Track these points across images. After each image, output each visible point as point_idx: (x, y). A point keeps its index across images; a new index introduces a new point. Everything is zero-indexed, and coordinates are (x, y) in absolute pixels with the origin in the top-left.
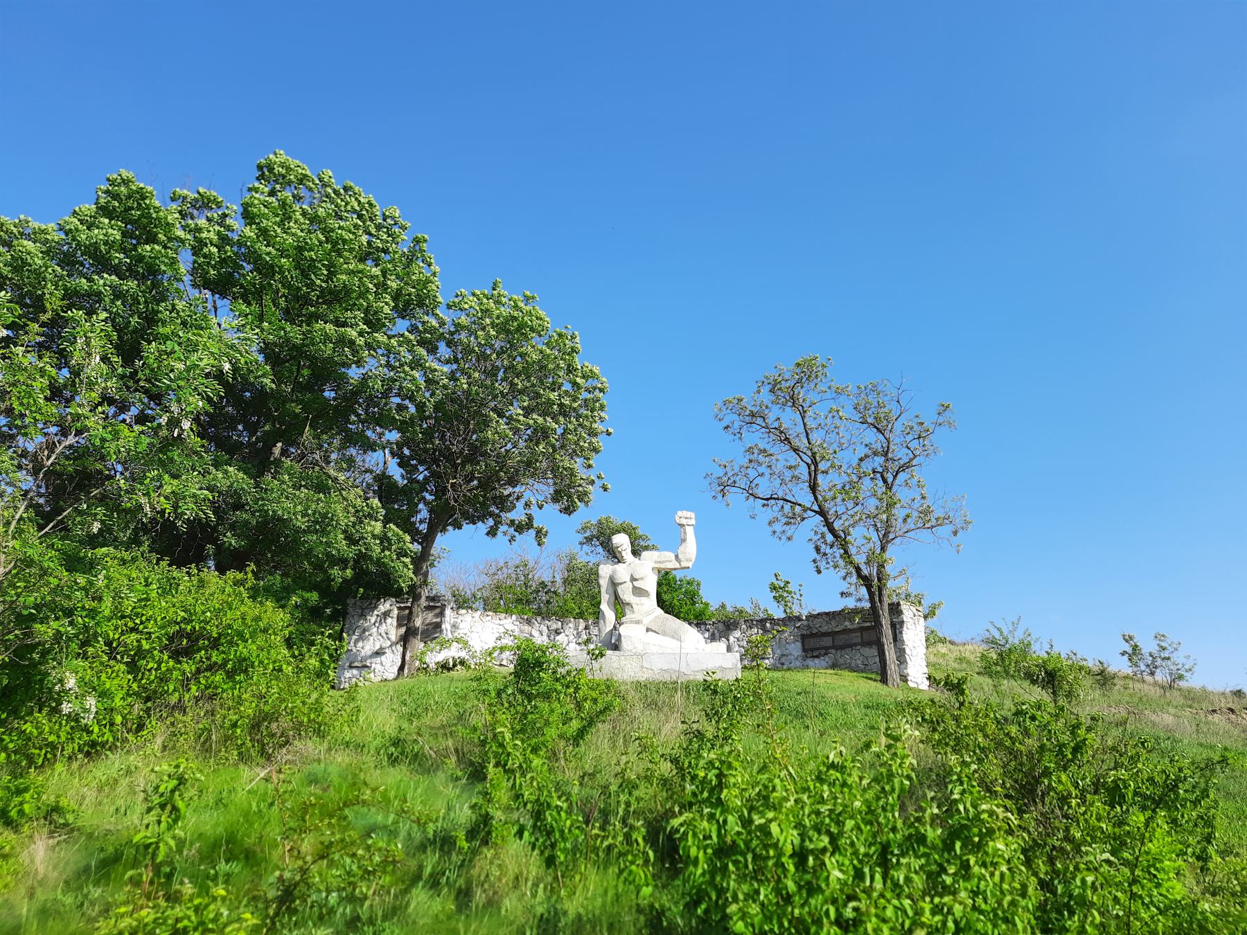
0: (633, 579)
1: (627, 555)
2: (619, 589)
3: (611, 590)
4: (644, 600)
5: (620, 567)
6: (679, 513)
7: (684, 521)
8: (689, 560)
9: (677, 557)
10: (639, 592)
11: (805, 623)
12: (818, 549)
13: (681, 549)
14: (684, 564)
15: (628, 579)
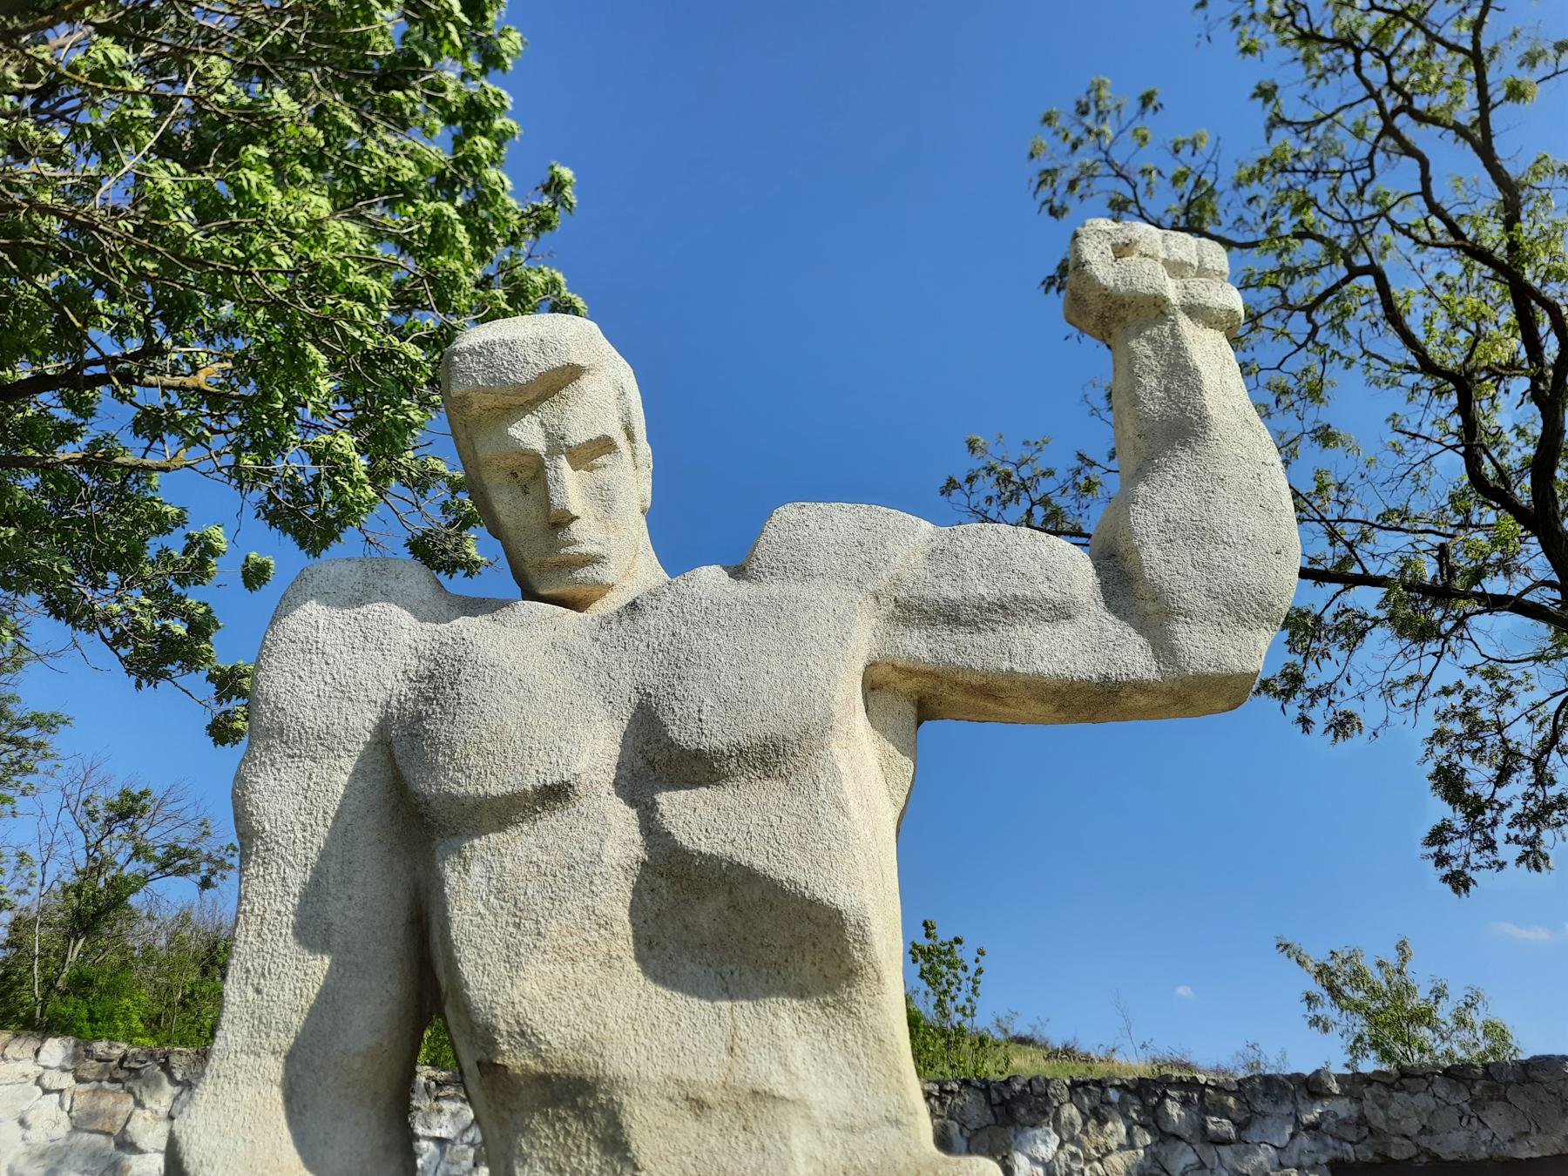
0: (658, 760)
1: (611, 515)
2: (471, 888)
3: (371, 897)
4: (782, 1041)
5: (517, 645)
8: (1239, 608)
9: (1121, 581)
10: (728, 930)
11: (1344, 1108)
12: (1449, 782)
14: (1208, 646)
15: (593, 751)
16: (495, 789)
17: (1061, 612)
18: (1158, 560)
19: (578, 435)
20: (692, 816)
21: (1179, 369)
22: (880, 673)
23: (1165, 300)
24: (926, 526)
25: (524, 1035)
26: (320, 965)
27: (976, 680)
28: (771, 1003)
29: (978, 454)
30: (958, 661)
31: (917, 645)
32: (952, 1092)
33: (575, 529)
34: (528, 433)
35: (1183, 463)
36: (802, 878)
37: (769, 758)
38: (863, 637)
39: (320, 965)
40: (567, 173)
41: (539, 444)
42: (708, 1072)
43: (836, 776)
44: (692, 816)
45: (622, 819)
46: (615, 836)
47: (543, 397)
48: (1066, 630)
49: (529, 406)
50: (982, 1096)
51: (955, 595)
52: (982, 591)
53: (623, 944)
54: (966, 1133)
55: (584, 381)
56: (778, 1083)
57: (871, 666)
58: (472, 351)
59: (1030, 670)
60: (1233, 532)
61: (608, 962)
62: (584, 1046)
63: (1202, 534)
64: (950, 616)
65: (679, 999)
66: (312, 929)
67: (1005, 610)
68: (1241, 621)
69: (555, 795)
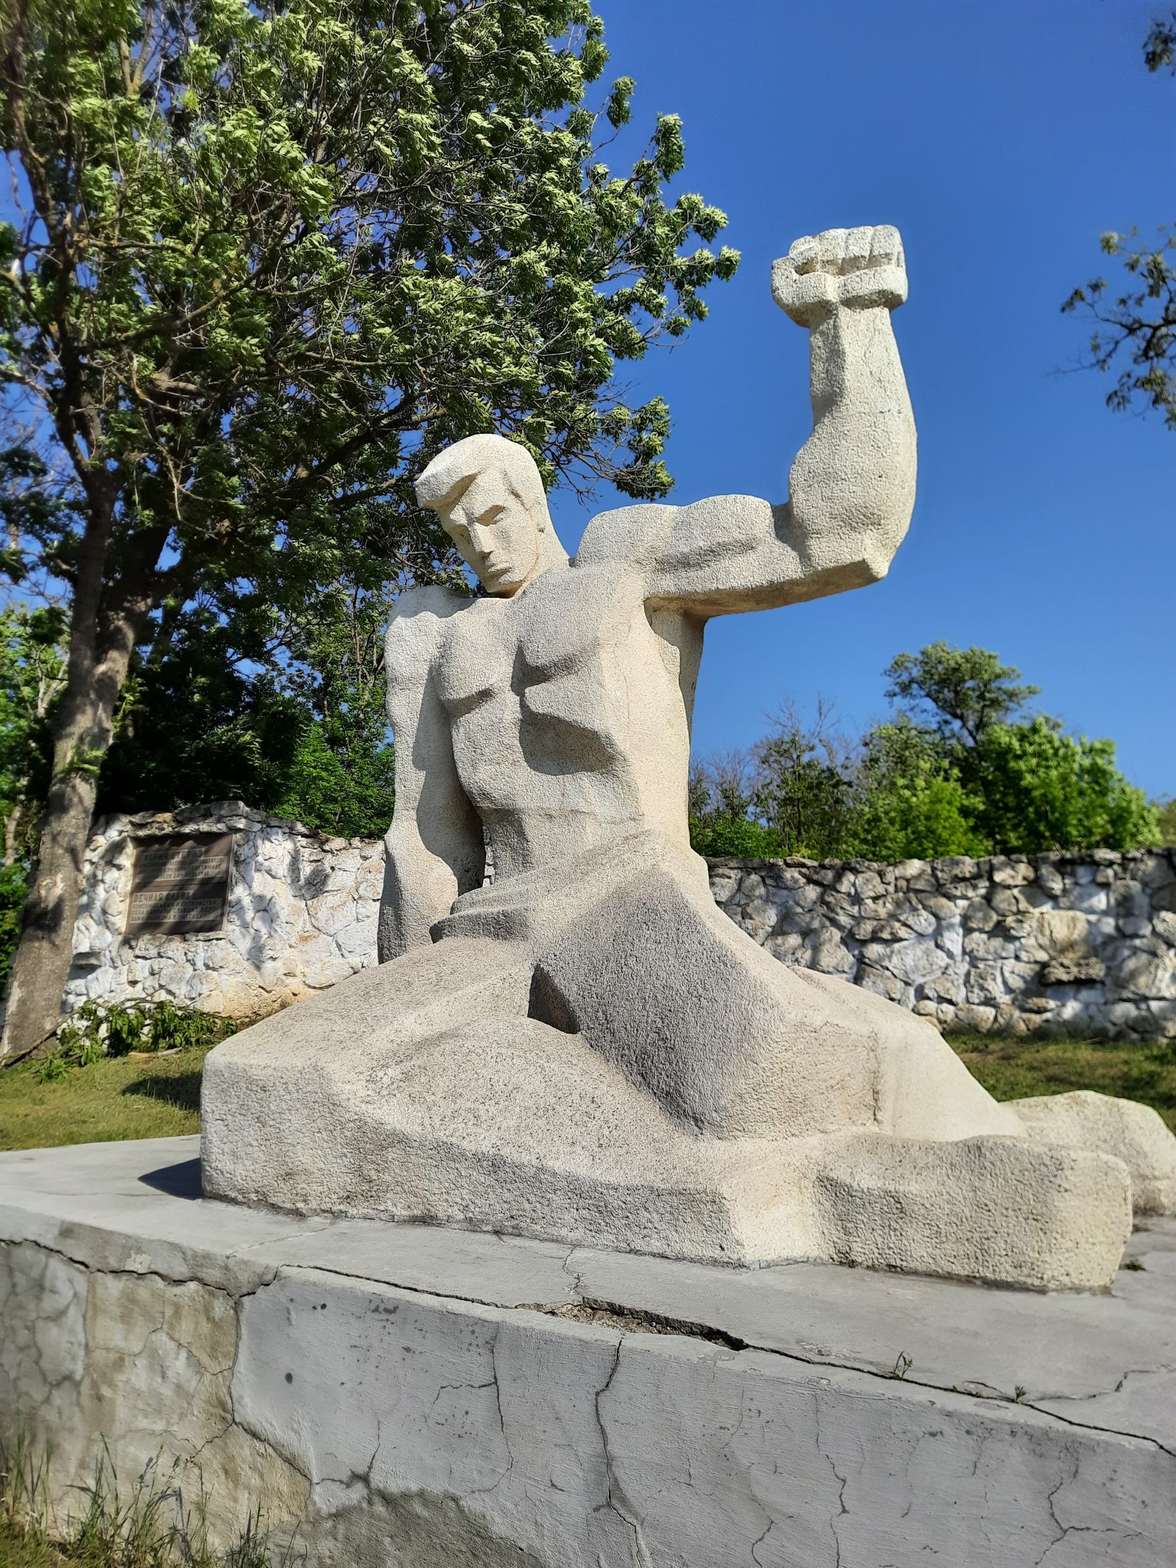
0: (527, 674)
6: (804, 247)
7: (830, 287)
9: (788, 526)
13: (811, 456)
14: (830, 551)
15: (500, 673)
16: (463, 696)
17: (747, 546)
18: (805, 504)
19: (480, 509)
20: (541, 698)
21: (835, 354)
22: (655, 602)
23: (828, 302)
24: (674, 508)
25: (485, 795)
26: (423, 774)
27: (702, 597)
28: (579, 775)
29: (1114, 252)
30: (689, 589)
31: (669, 584)
32: (1134, 859)
33: (493, 558)
34: (458, 516)
35: (826, 427)
36: (578, 719)
37: (567, 665)
38: (635, 587)
39: (423, 774)
40: (672, 119)
41: (463, 520)
42: (552, 804)
43: (600, 667)
44: (541, 698)
45: (512, 699)
46: (507, 708)
47: (461, 495)
48: (751, 556)
49: (456, 501)
50: (1164, 862)
51: (686, 550)
52: (701, 544)
53: (519, 755)
54: (1148, 891)
55: (479, 480)
56: (582, 806)
57: (646, 601)
58: (422, 484)
59: (728, 586)
60: (848, 471)
61: (514, 763)
62: (507, 797)
63: (830, 476)
64: (685, 563)
65: (544, 776)
66: (418, 763)
67: (713, 553)
68: (853, 529)
69: (485, 695)
